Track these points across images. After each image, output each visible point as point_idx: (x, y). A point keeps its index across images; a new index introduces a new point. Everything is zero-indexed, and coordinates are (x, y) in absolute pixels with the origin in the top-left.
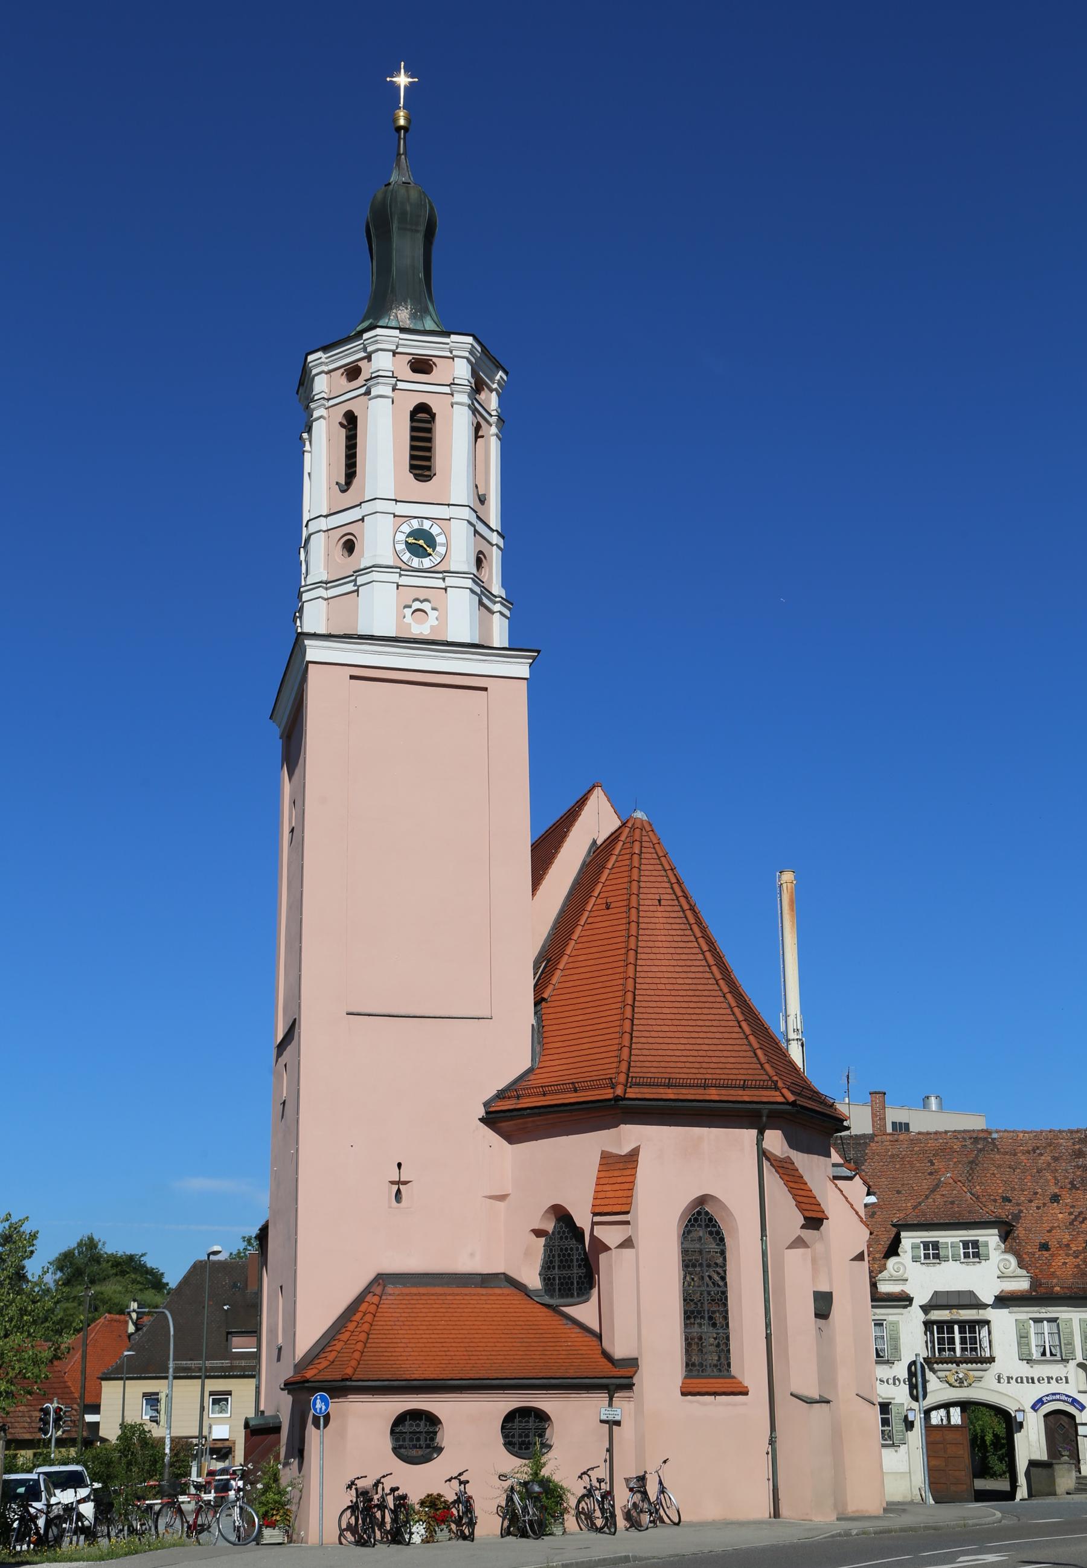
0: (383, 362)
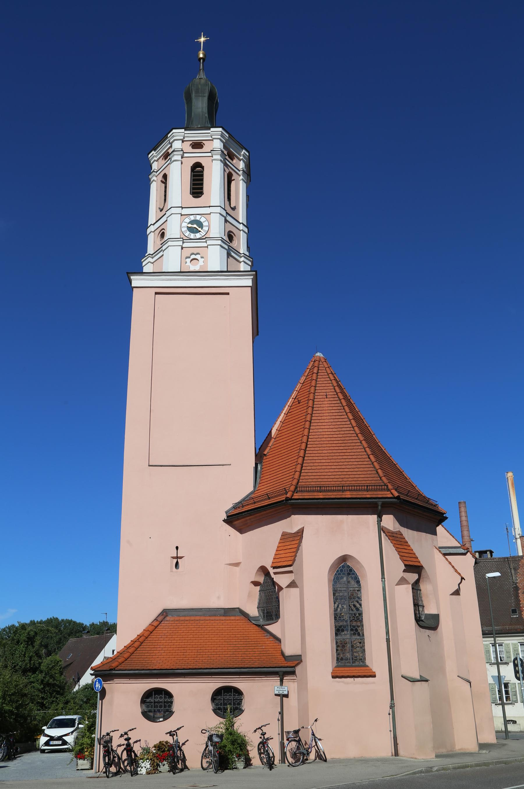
0: (177, 145)
